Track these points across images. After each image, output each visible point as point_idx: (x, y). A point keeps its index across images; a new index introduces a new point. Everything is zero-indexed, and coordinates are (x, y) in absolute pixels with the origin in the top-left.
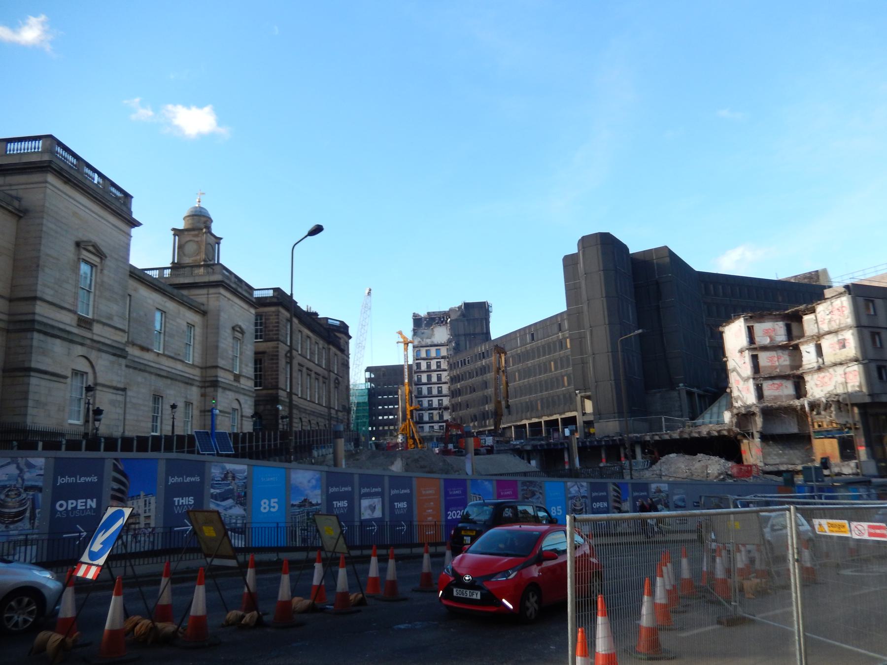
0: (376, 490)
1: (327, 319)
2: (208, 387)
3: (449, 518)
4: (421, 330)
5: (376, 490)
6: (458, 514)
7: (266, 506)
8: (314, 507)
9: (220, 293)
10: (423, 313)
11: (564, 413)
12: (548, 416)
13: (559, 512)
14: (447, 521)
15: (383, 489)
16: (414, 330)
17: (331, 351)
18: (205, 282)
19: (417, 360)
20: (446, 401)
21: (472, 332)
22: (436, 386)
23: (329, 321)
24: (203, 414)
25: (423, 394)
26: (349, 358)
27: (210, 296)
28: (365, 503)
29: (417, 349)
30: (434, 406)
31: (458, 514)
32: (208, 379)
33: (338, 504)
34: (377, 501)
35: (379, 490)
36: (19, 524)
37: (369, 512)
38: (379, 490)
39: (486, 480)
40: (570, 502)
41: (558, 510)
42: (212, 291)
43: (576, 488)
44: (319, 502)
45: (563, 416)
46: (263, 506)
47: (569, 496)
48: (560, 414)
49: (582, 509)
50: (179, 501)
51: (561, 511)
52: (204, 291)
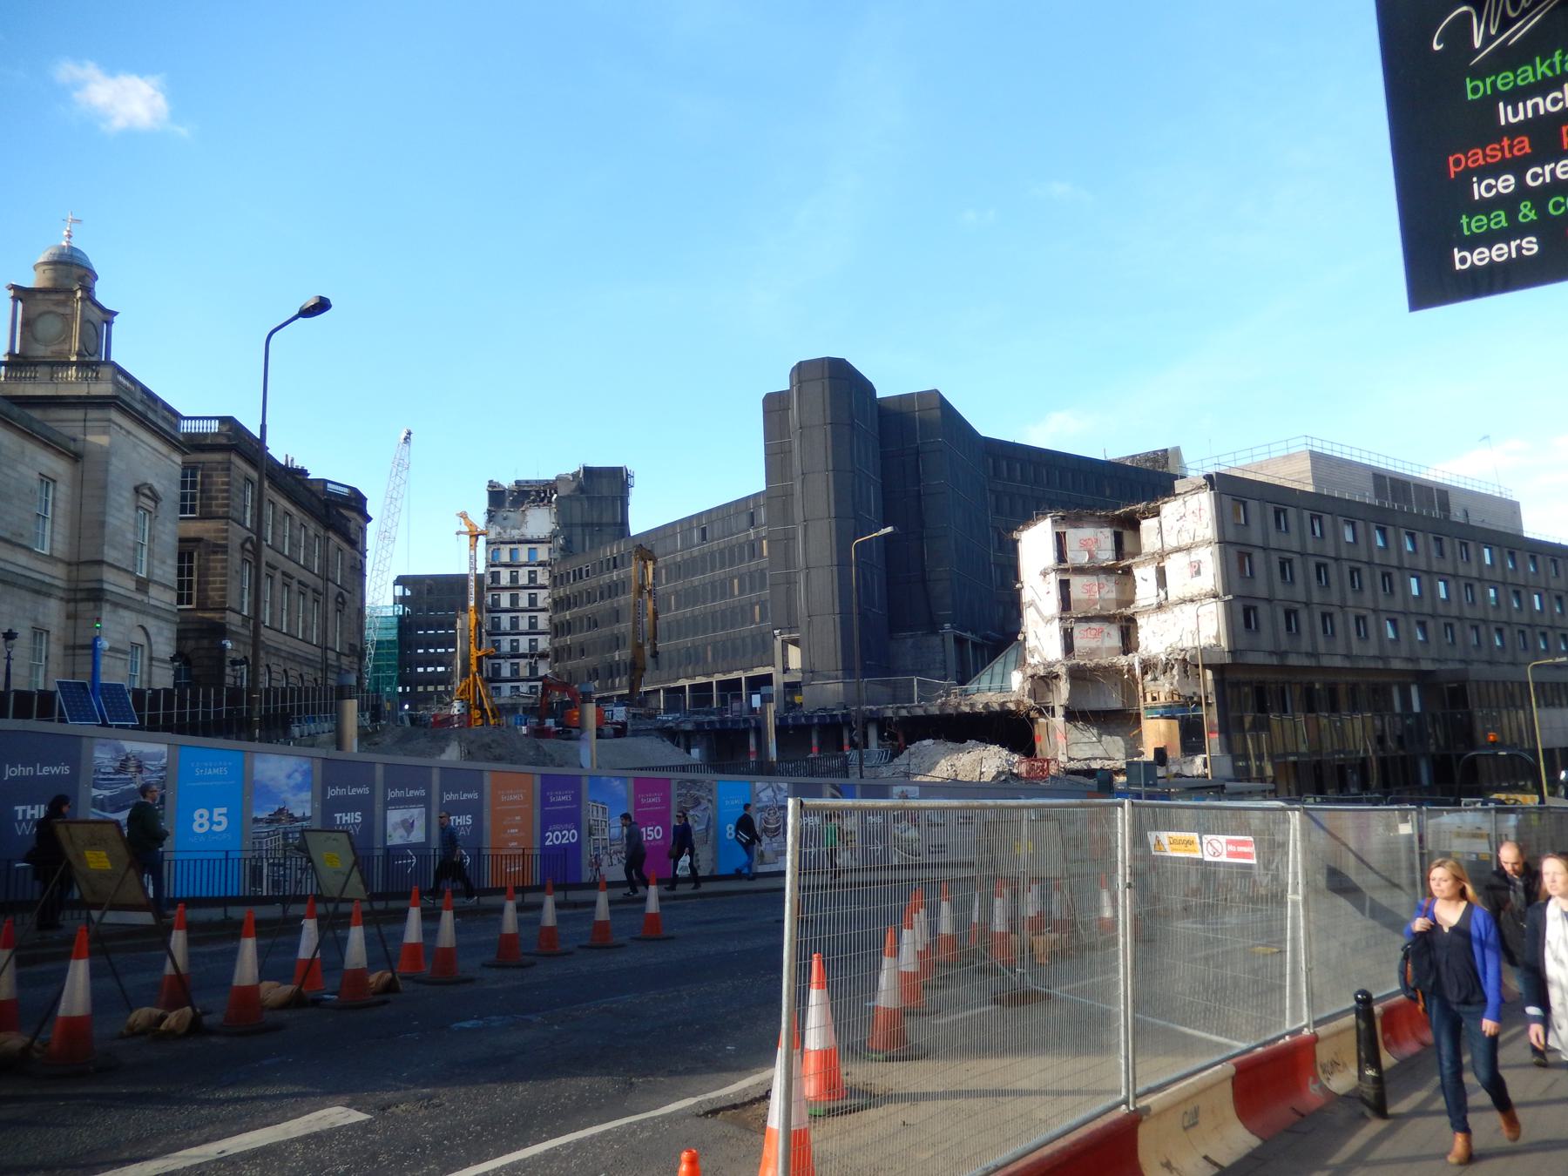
0: (417, 793)
1: (325, 482)
2: (82, 600)
3: (548, 843)
4: (503, 513)
5: (417, 793)
6: (563, 836)
7: (204, 820)
8: (297, 824)
9: (109, 420)
10: (507, 482)
11: (752, 668)
12: (724, 673)
13: (219, 823)
14: (543, 847)
15: (429, 794)
16: (489, 512)
17: (331, 543)
18: (79, 397)
19: (492, 566)
20: (543, 643)
21: (595, 521)
22: (527, 615)
23: (329, 485)
24: (70, 652)
25: (502, 628)
26: (365, 557)
27: (88, 424)
28: (395, 816)
29: (493, 547)
30: (521, 651)
31: (563, 836)
32: (82, 585)
33: (457, 821)
34: (416, 814)
35: (422, 793)
36: (777, 838)
37: (401, 832)
38: (422, 793)
39: (617, 778)
40: (759, 815)
41: (216, 818)
42: (94, 414)
43: (769, 792)
44: (308, 814)
45: (750, 674)
46: (198, 821)
47: (758, 805)
48: (745, 670)
49: (778, 828)
50: (341, 818)
51: (224, 820)
52: (78, 414)
